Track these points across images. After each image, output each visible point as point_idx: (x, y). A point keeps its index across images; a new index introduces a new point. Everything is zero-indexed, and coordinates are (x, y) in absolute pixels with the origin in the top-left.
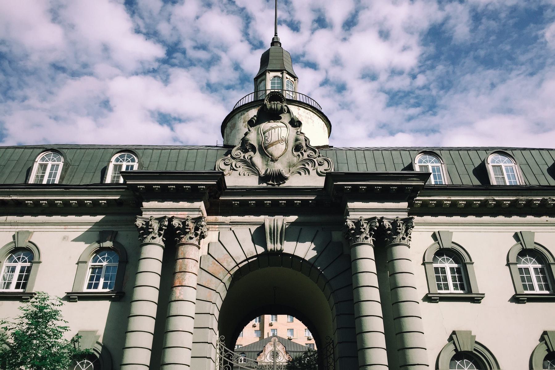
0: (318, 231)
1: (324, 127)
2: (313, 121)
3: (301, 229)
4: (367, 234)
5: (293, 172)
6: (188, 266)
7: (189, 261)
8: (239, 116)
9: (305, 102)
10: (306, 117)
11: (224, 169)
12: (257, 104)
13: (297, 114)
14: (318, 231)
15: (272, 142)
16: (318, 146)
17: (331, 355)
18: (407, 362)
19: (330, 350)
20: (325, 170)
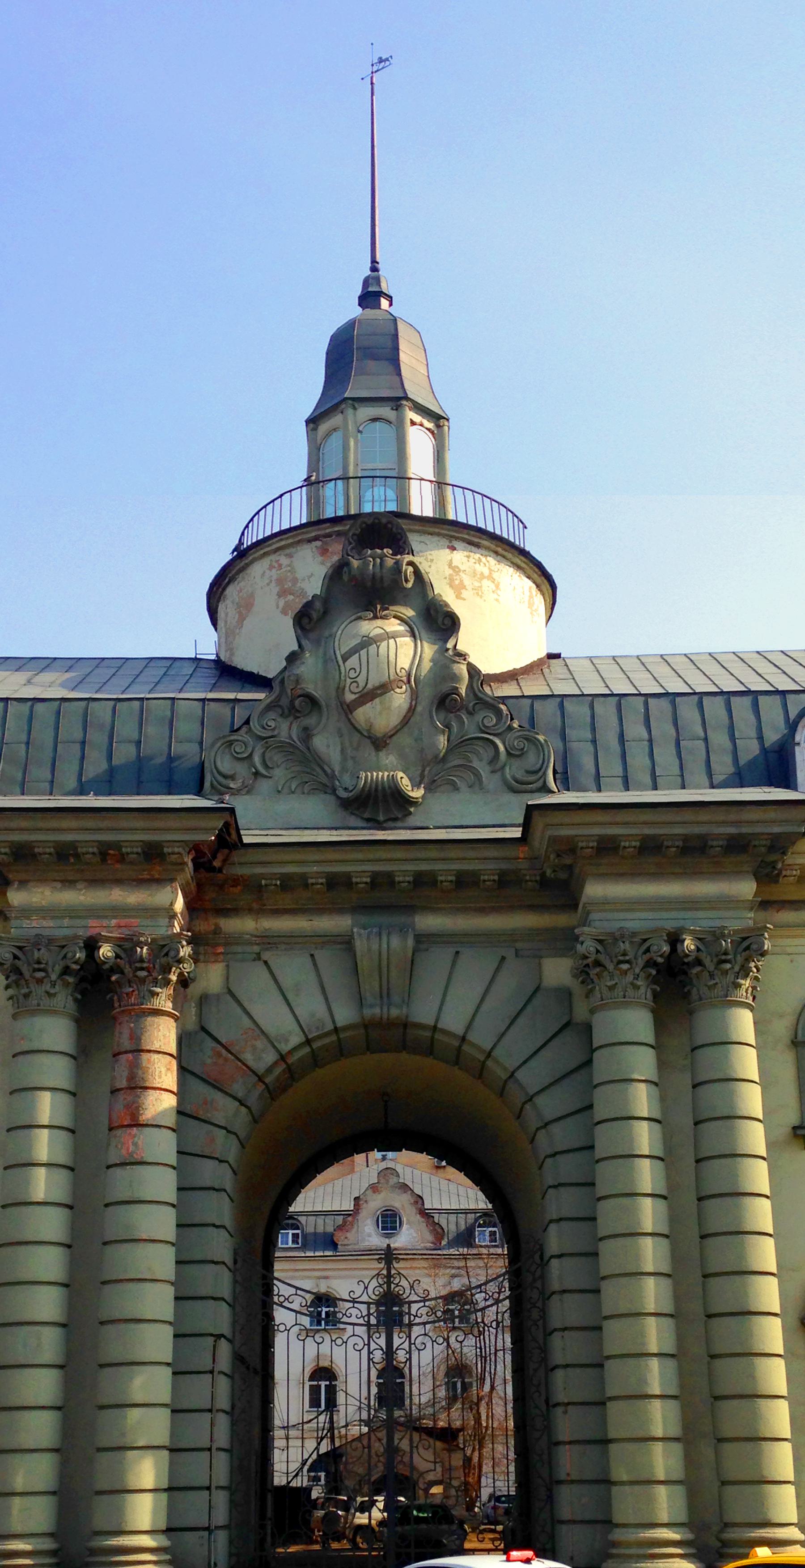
0: (503, 958)
1: (531, 597)
2: (497, 586)
3: (457, 953)
4: (638, 975)
5: (435, 781)
6: (151, 1070)
7: (152, 1059)
8: (264, 572)
9: (472, 522)
10: (475, 572)
11: (230, 773)
12: (319, 533)
13: (447, 567)
14: (503, 958)
15: (370, 686)
16: (511, 668)
17: (534, 1280)
18: (646, 1383)
19: (533, 1269)
20: (528, 772)
